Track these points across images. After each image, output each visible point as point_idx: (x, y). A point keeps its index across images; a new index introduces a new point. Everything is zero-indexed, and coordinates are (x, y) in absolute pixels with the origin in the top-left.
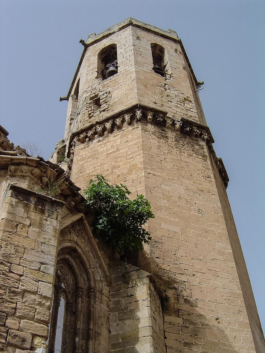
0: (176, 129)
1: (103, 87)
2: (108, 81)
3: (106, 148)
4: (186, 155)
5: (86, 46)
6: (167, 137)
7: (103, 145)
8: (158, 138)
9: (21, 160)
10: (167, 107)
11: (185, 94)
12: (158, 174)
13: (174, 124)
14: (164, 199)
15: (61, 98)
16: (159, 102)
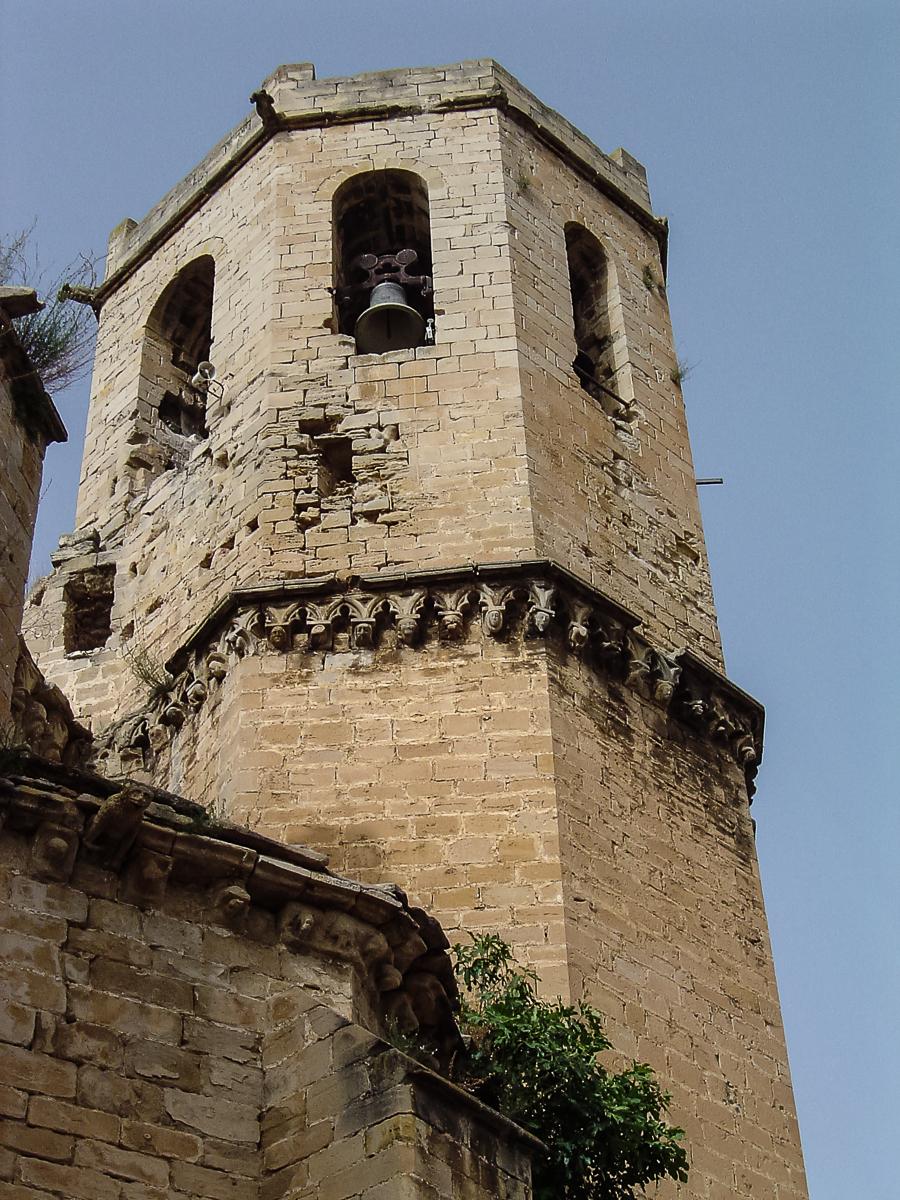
0: (657, 695)
1: (367, 392)
2: (389, 371)
3: (389, 717)
4: (687, 825)
5: (276, 125)
6: (628, 732)
7: (374, 698)
8: (602, 730)
9: (340, 896)
10: (623, 578)
11: (678, 516)
12: (605, 906)
13: (653, 676)
14: (624, 1025)
15: (66, 288)
16: (600, 552)
